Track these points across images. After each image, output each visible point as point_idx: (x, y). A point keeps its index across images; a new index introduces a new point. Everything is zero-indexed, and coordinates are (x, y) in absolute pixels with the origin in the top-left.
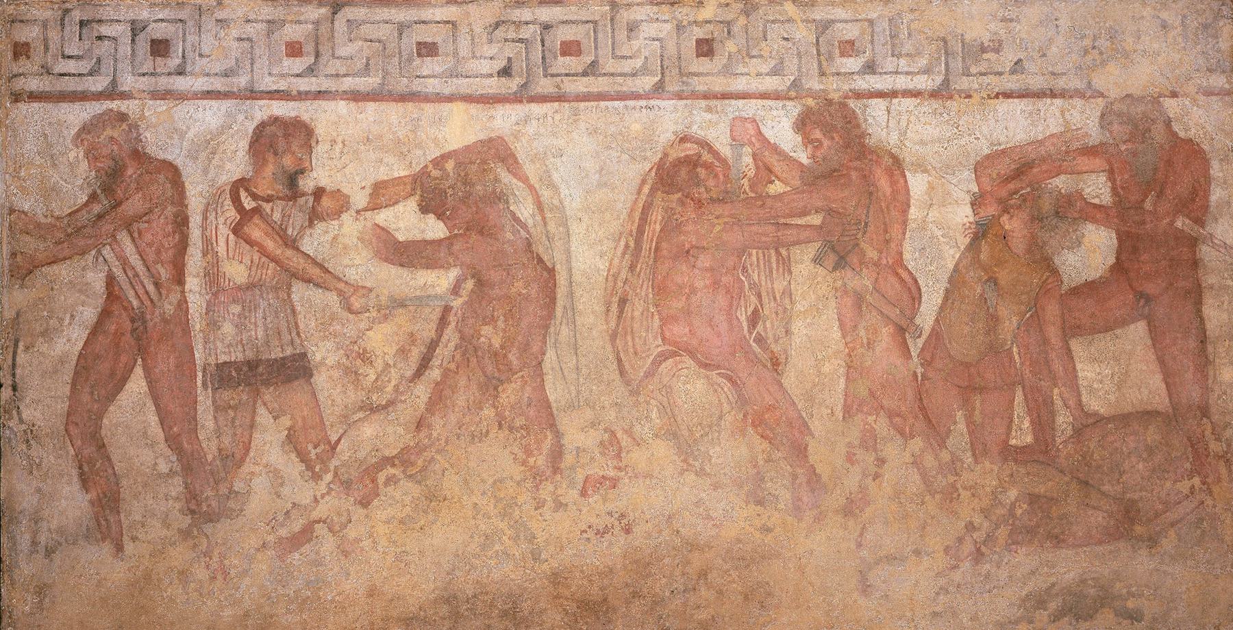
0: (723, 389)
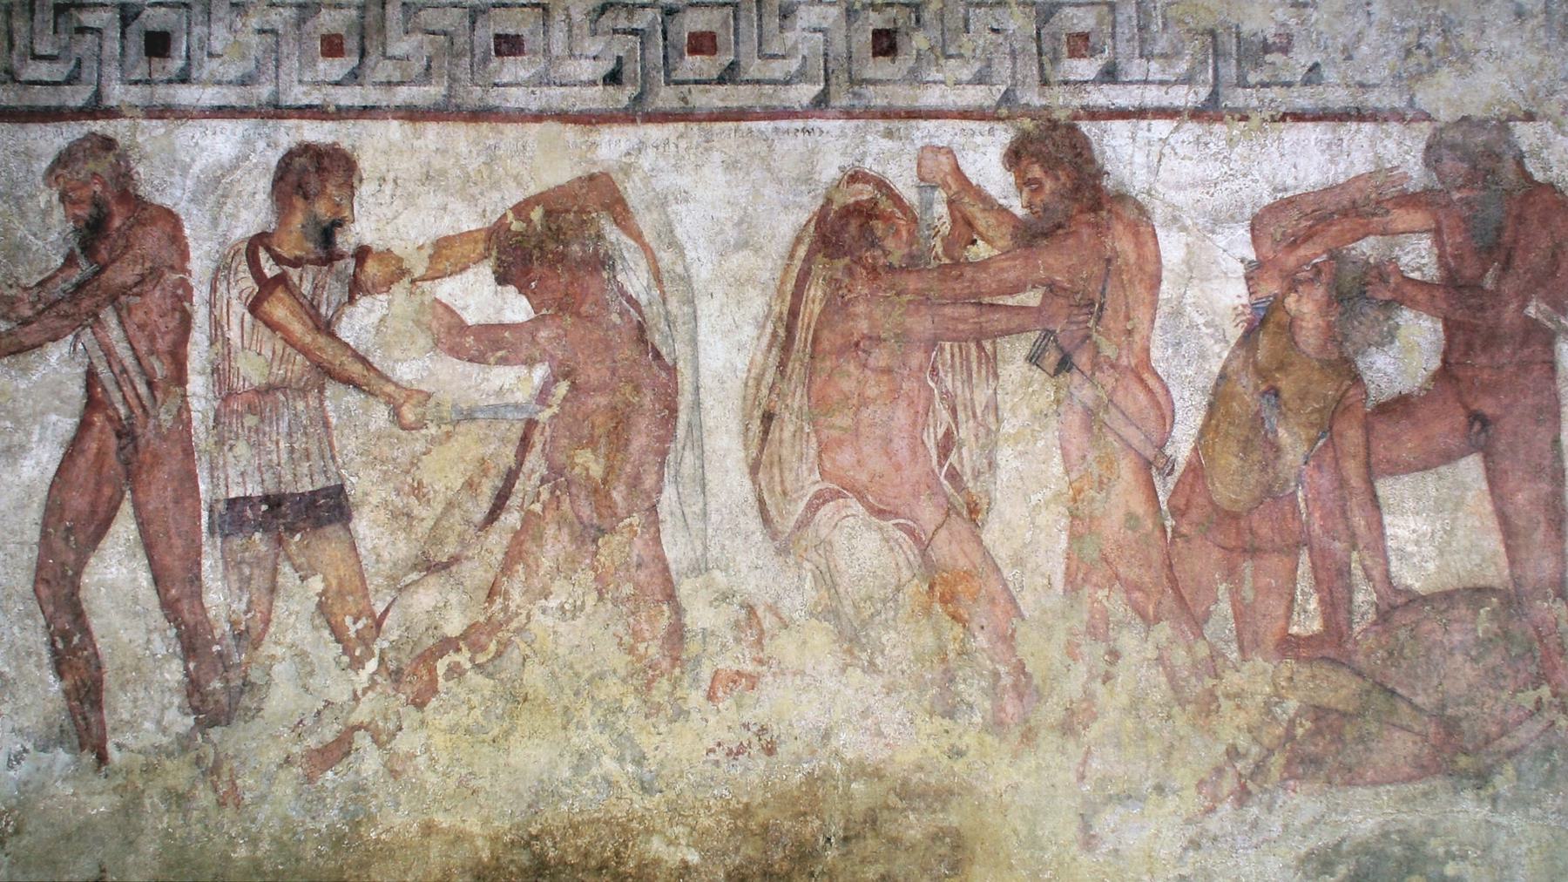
0: (901, 547)
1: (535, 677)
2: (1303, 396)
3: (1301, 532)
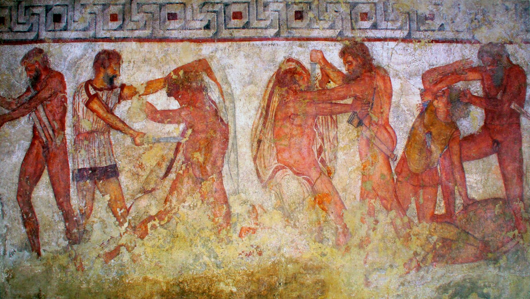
0: (305, 185)
1: (181, 229)
2: (439, 135)
3: (439, 180)
